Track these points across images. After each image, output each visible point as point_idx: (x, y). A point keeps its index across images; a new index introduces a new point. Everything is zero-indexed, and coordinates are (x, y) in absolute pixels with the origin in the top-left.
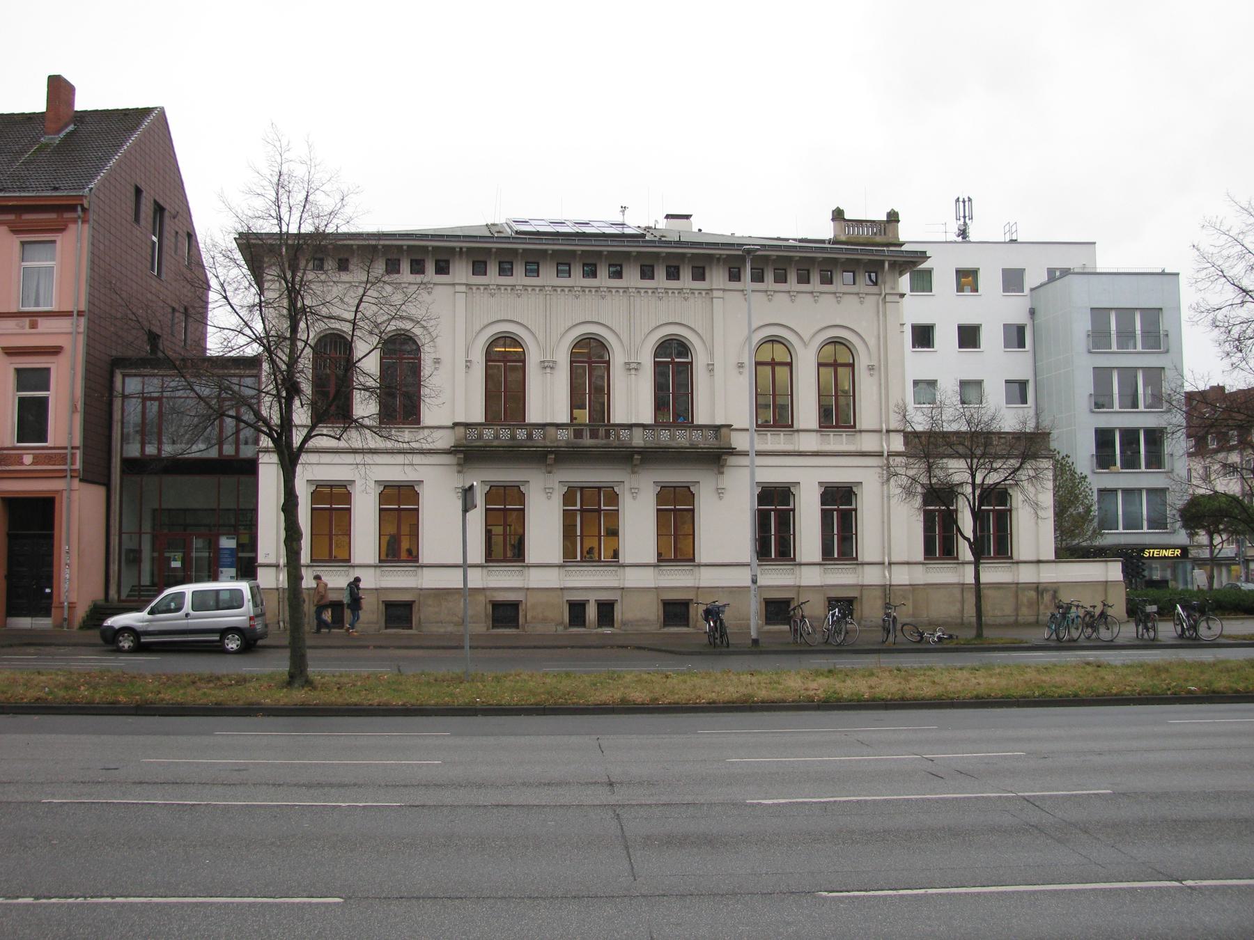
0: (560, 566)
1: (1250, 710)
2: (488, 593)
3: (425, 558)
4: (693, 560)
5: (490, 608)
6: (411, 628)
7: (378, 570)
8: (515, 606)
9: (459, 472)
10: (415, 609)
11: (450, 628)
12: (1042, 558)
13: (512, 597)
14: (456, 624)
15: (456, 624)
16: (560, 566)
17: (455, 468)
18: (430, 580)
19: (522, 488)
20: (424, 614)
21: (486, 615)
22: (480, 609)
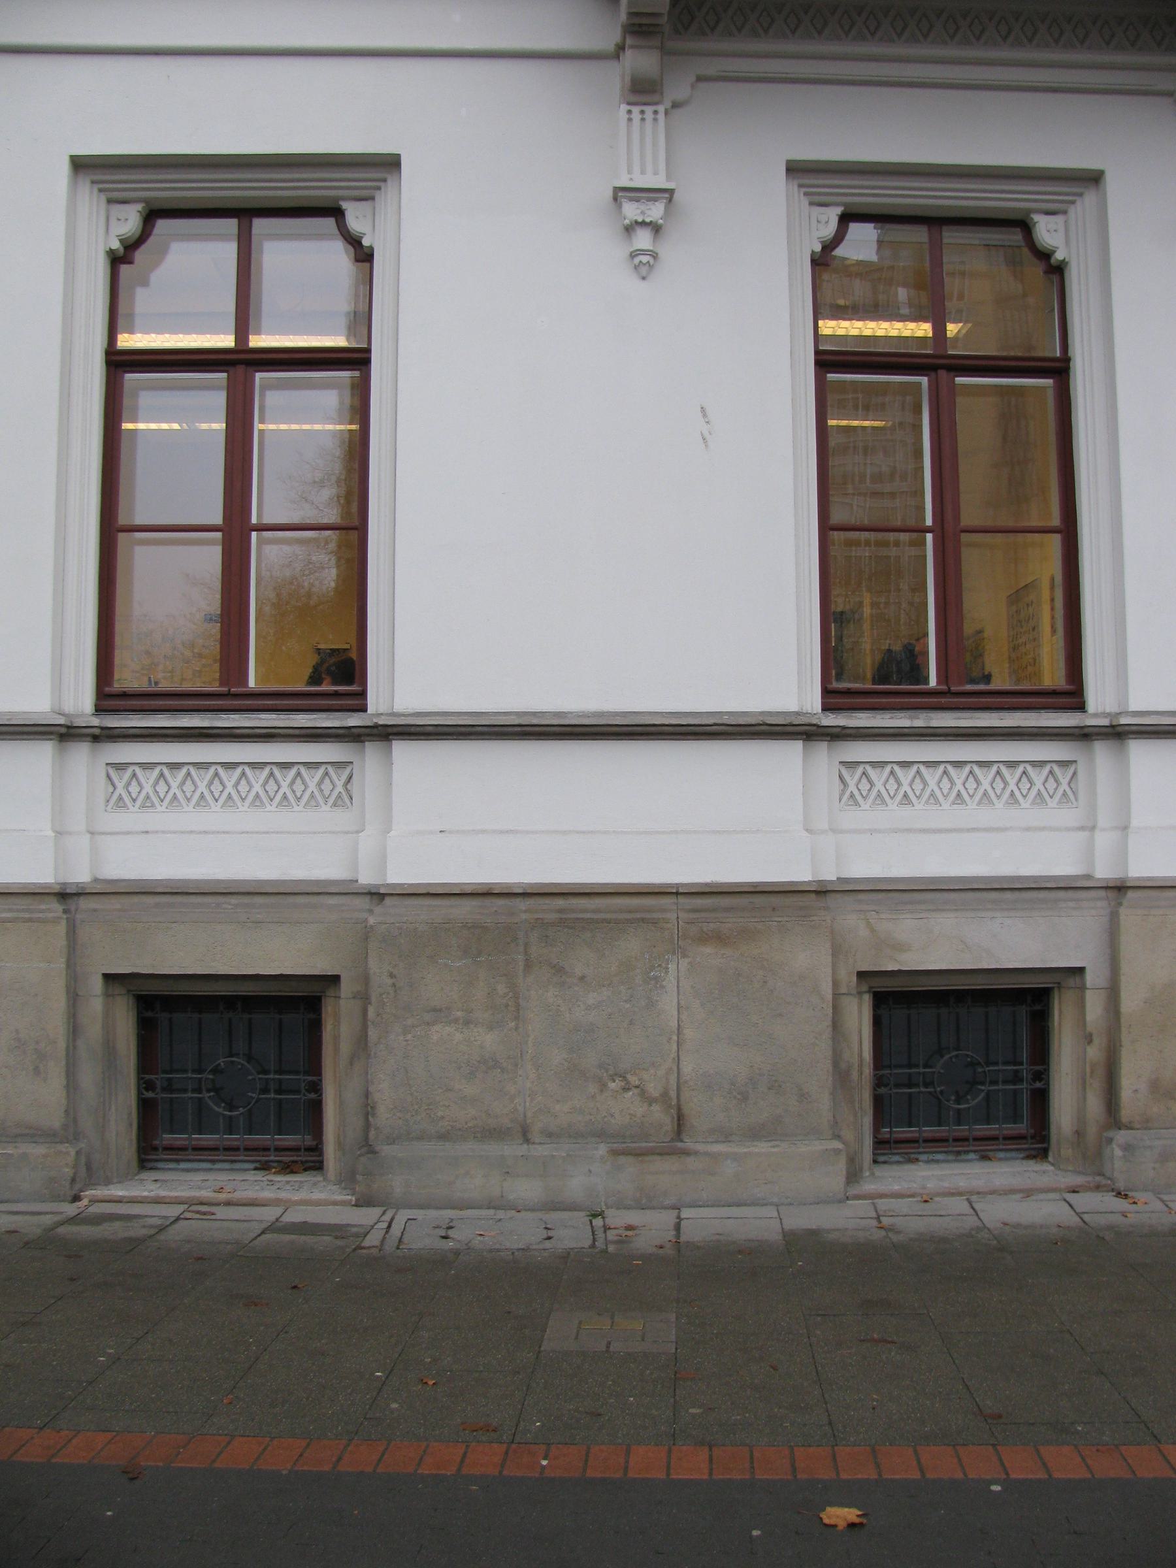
0: (65, 734)
1: (1170, 69)
2: (851, 920)
3: (401, 680)
4: (1072, 695)
5: (859, 1018)
6: (309, 1159)
7: (825, 757)
8: (1022, 1006)
9: (642, 91)
10: (339, 1025)
11: (589, 1176)
12: (44, 752)
13: (1010, 945)
14: (630, 1146)
15: (630, 1146)
16: (65, 734)
17: (612, 78)
18: (440, 825)
19: (1047, 232)
20: (394, 1067)
21: (841, 1076)
22: (817, 1034)
